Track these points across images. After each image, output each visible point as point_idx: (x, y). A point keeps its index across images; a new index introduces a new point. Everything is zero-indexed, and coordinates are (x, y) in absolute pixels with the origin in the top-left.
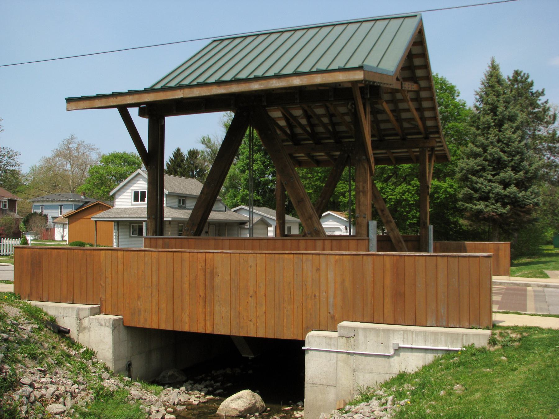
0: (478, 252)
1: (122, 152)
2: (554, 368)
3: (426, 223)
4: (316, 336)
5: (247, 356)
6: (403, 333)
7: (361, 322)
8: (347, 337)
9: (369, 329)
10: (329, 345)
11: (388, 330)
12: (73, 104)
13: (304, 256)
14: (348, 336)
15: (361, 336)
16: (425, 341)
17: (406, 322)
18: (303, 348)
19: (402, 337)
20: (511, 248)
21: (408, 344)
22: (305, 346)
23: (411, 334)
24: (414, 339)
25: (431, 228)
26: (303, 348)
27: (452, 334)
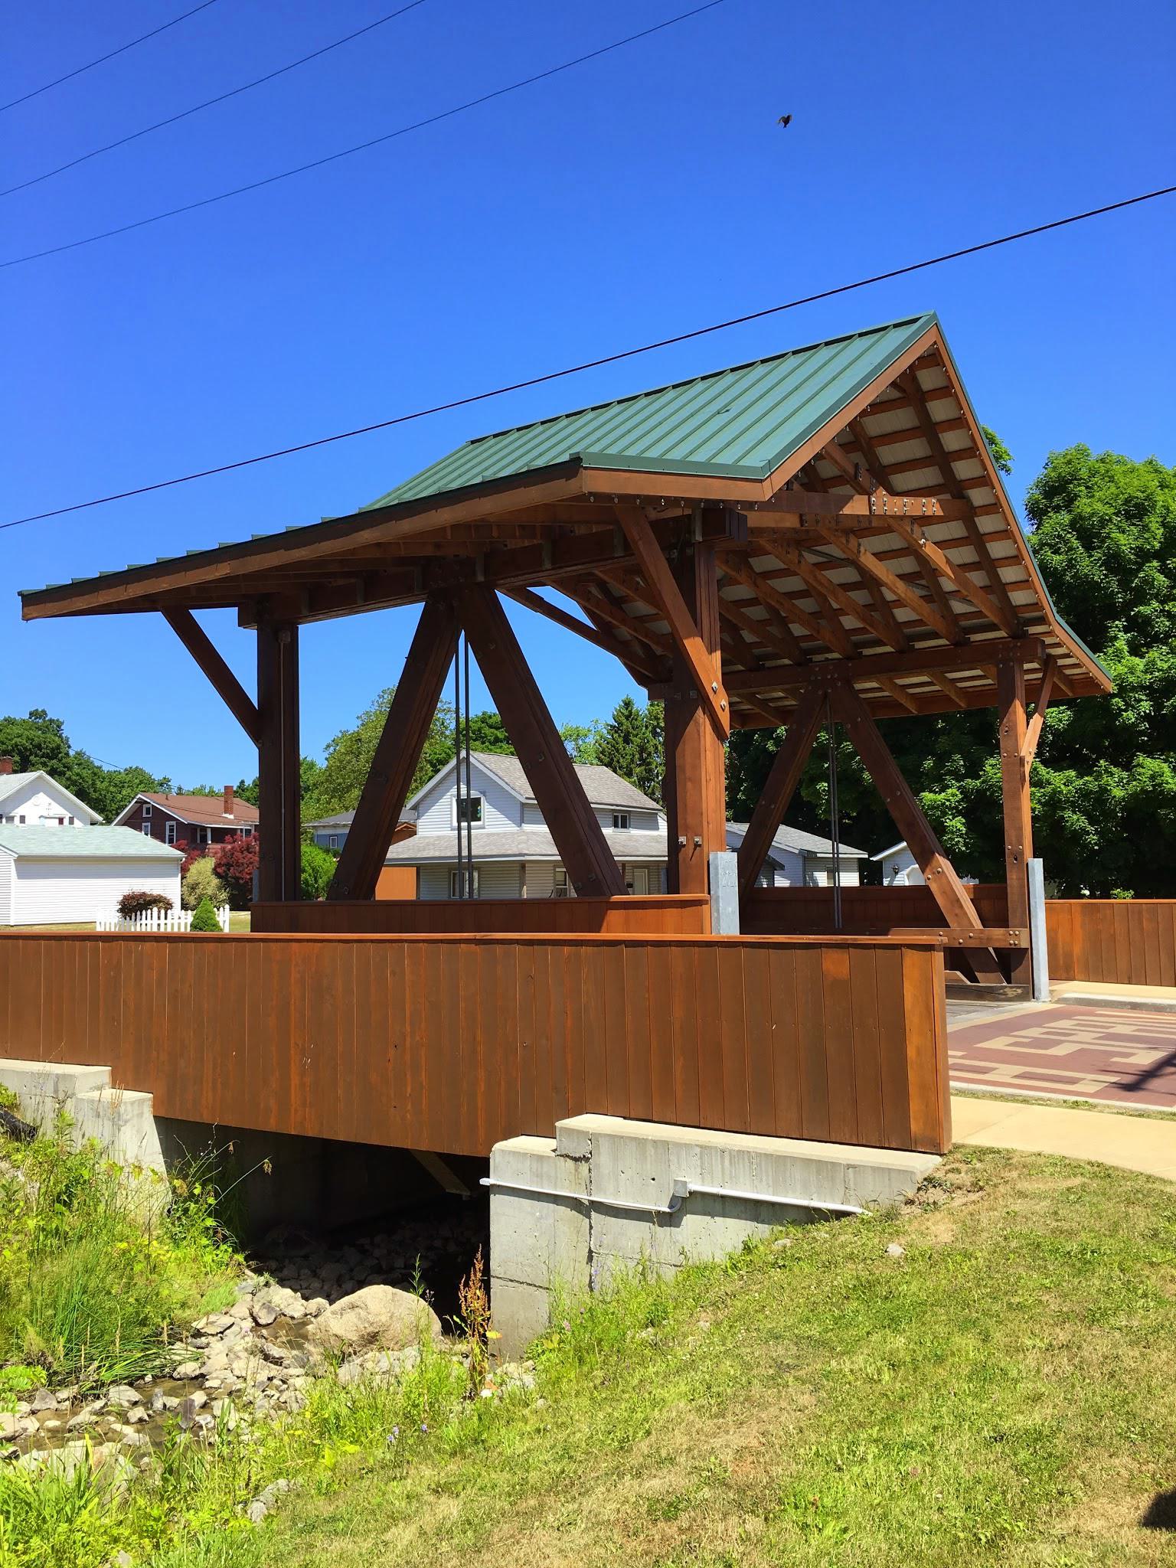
0: (1020, 819)
1: (22, 714)
2: (508, 1476)
3: (1022, 853)
4: (510, 1152)
5: (458, 1192)
6: (701, 1153)
7: (625, 1118)
8: (576, 1160)
9: (622, 1137)
10: (539, 1176)
11: (664, 1145)
12: (1036, 994)
13: (498, 948)
14: (577, 1155)
15: (603, 1159)
16: (703, 1181)
17: (805, 1131)
18: (484, 1181)
19: (699, 1163)
20: (803, 469)
21: (834, 1201)
22: (488, 1176)
23: (887, 1174)
24: (727, 1172)
25: (1037, 866)
26: (484, 1181)
27: (819, 1165)
